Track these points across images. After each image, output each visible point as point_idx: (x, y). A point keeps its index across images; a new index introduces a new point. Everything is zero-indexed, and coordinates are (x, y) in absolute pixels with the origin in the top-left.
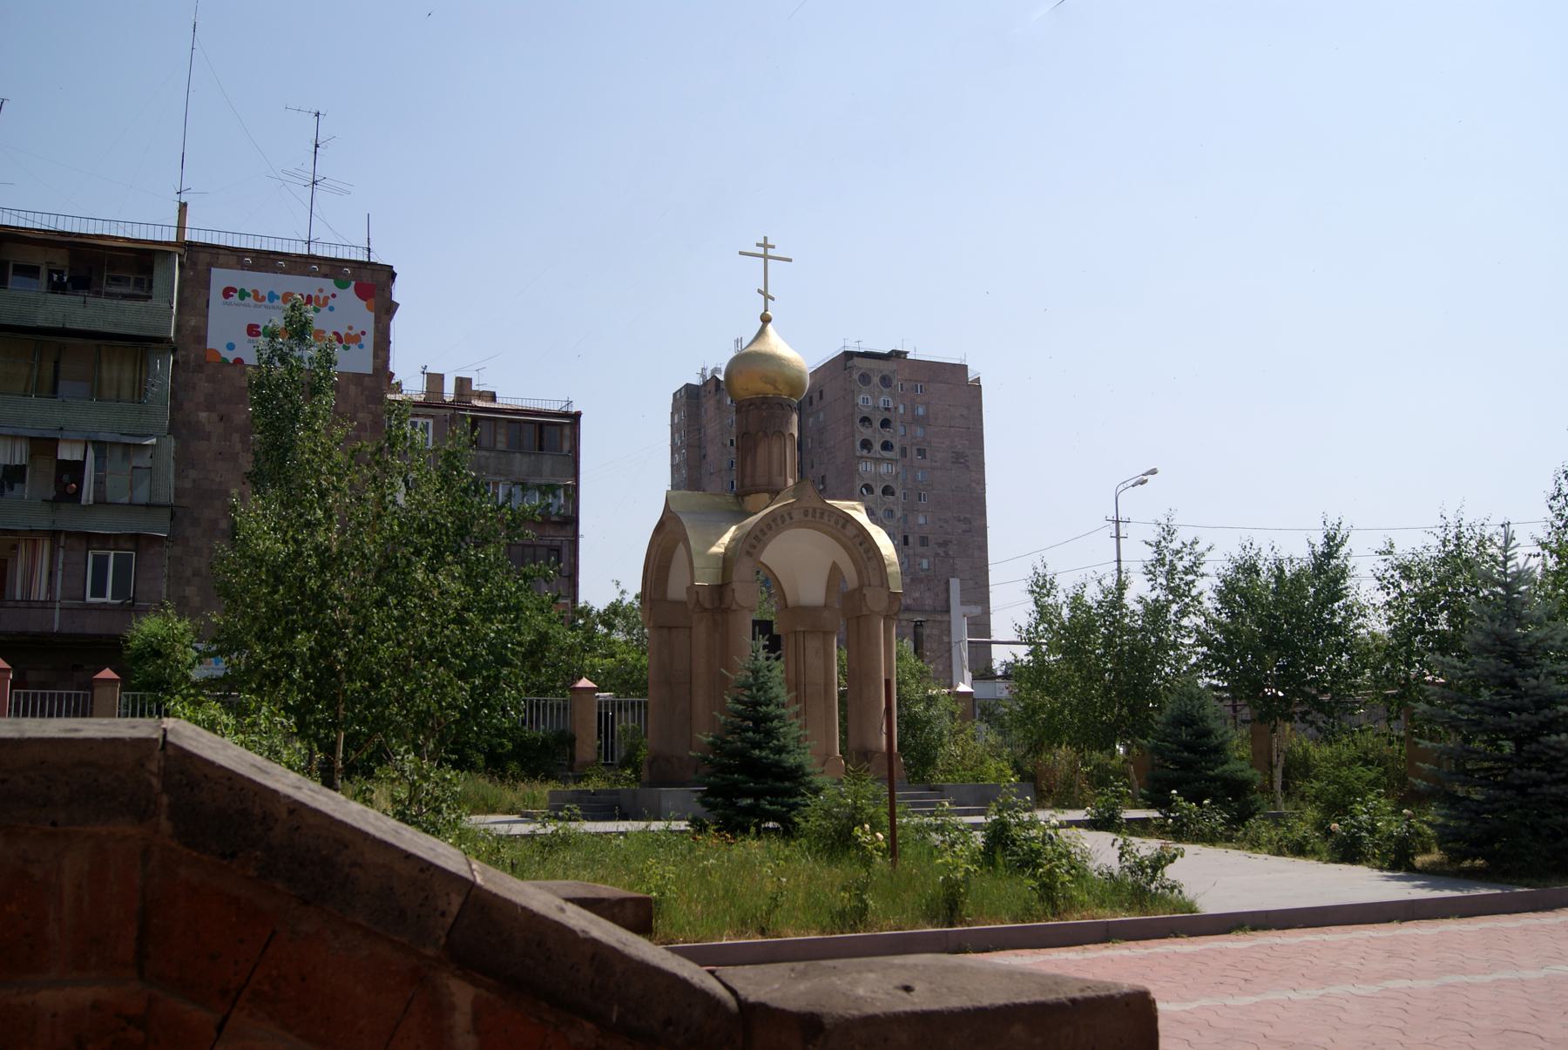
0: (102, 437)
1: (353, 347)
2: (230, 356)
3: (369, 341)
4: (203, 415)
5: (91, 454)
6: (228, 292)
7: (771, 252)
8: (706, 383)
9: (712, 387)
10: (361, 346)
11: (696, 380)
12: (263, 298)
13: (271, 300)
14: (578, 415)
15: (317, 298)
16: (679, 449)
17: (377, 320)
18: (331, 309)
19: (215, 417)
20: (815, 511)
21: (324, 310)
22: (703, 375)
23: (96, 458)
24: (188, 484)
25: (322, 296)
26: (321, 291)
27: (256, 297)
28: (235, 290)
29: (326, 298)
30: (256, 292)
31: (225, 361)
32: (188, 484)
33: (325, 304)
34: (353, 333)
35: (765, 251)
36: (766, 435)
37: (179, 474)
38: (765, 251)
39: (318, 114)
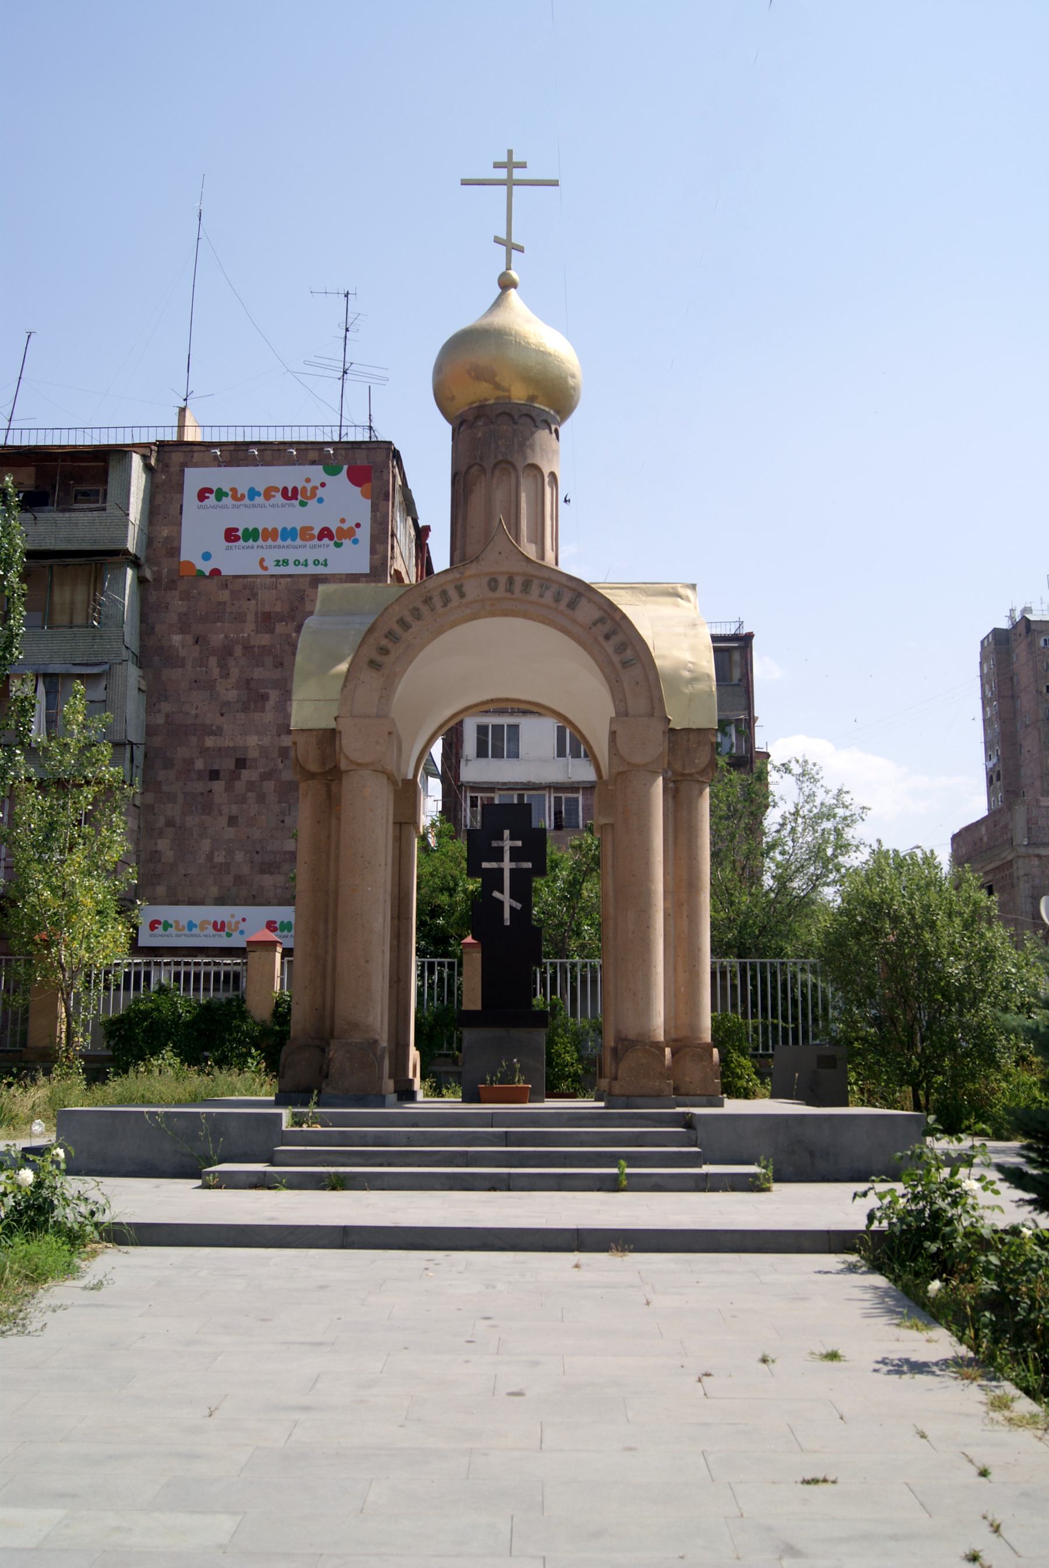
0: (51, 669)
1: (347, 543)
2: (206, 568)
3: (364, 535)
4: (177, 638)
5: (41, 688)
6: (203, 495)
7: (518, 174)
8: (1015, 626)
9: (1022, 629)
10: (356, 542)
11: (1005, 624)
12: (243, 497)
13: (251, 498)
14: (750, 636)
15: (304, 489)
16: (990, 700)
17: (375, 508)
18: (321, 501)
19: (189, 639)
20: (511, 581)
21: (312, 503)
22: (1011, 618)
23: (47, 693)
24: (160, 720)
25: (309, 486)
26: (308, 480)
27: (235, 497)
28: (211, 491)
29: (315, 488)
30: (234, 490)
31: (200, 574)
32: (160, 720)
33: (313, 495)
34: (345, 526)
35: (509, 175)
36: (483, 470)
37: (150, 708)
38: (509, 175)
39: (347, 295)
